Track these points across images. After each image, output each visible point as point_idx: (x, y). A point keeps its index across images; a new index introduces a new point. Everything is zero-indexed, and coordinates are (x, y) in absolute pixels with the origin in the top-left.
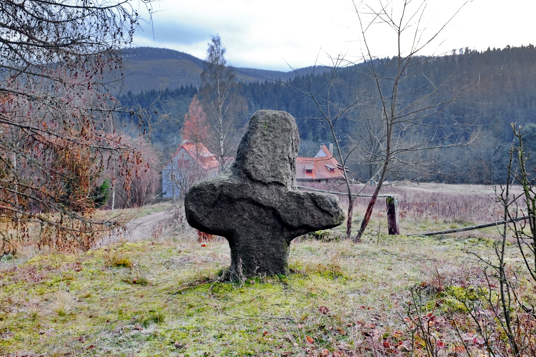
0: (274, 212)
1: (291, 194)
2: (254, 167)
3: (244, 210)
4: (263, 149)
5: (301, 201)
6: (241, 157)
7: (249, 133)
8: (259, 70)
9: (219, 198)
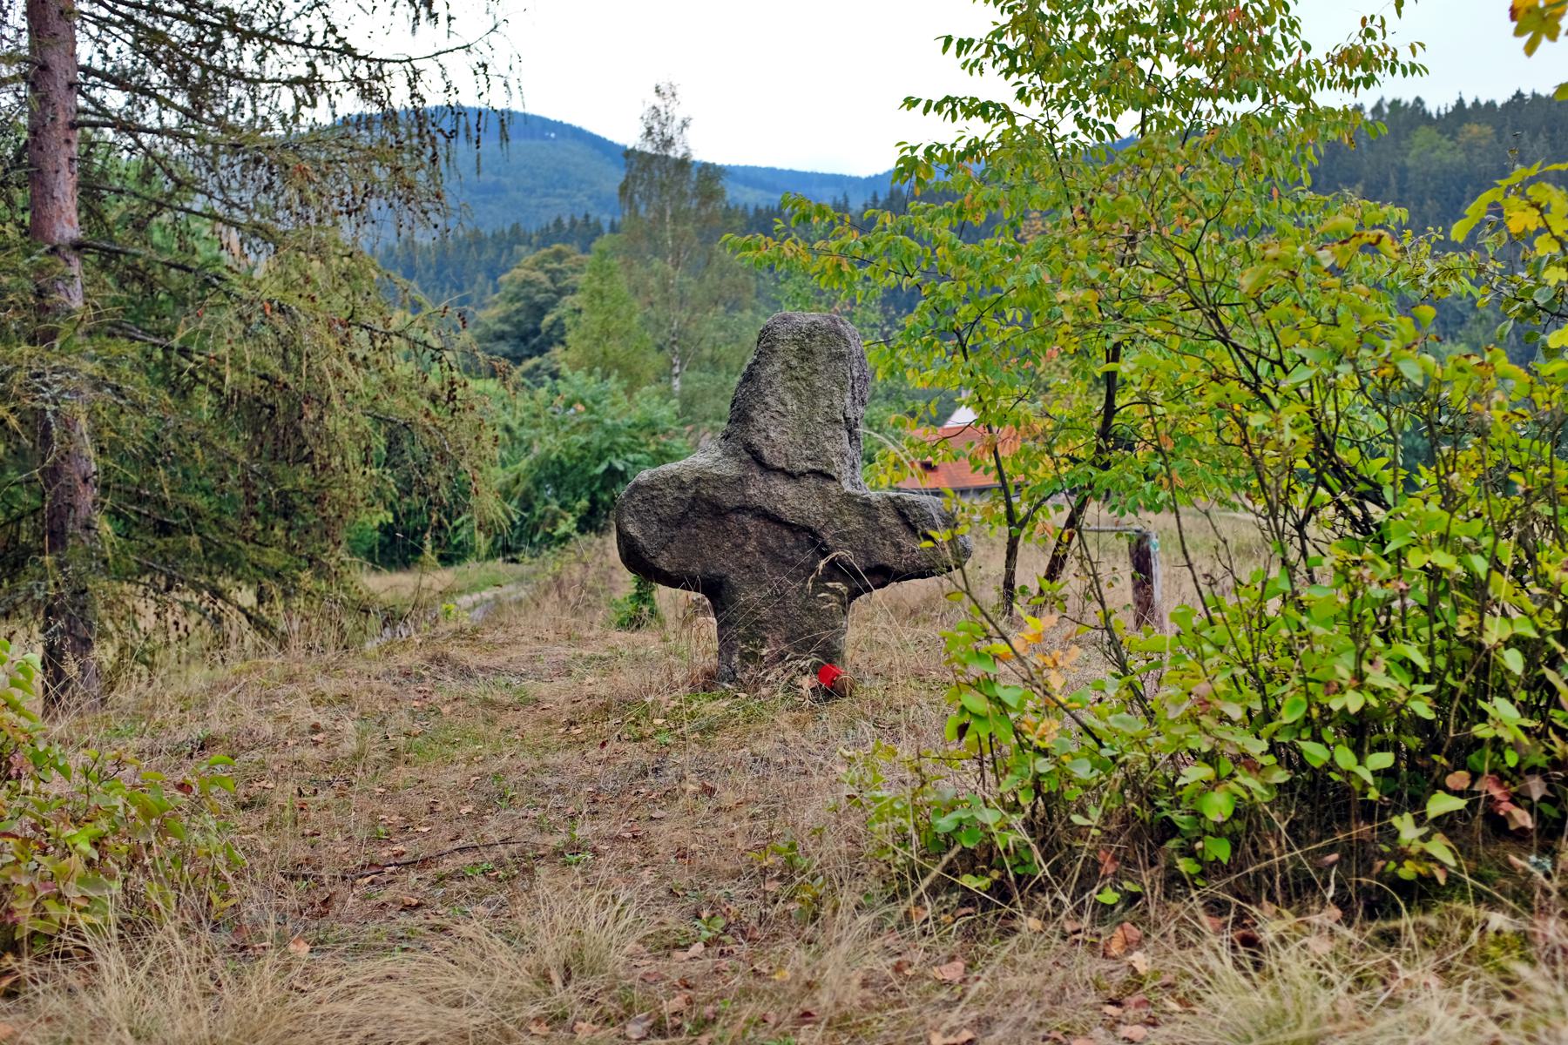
1: (849, 499)
2: (767, 437)
3: (746, 533)
4: (788, 397)
5: (873, 512)
6: (741, 415)
7: (756, 362)
8: (782, 171)
9: (692, 508)
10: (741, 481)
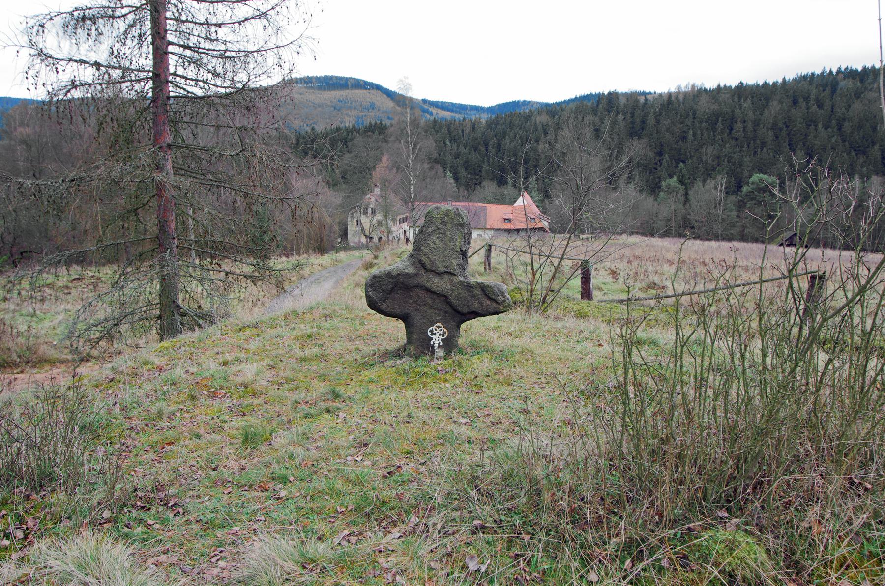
0: (444, 297)
4: (437, 241)
9: (396, 286)
10: (416, 275)
